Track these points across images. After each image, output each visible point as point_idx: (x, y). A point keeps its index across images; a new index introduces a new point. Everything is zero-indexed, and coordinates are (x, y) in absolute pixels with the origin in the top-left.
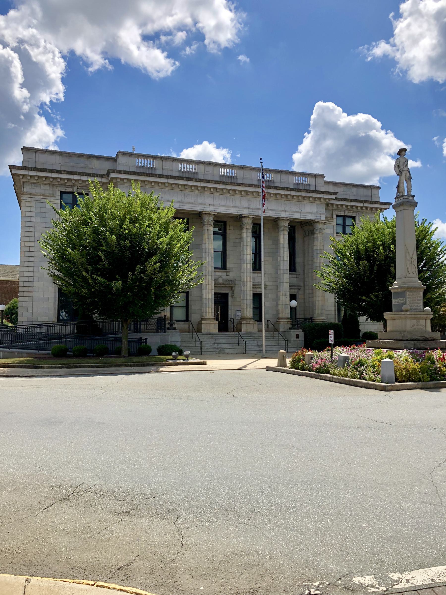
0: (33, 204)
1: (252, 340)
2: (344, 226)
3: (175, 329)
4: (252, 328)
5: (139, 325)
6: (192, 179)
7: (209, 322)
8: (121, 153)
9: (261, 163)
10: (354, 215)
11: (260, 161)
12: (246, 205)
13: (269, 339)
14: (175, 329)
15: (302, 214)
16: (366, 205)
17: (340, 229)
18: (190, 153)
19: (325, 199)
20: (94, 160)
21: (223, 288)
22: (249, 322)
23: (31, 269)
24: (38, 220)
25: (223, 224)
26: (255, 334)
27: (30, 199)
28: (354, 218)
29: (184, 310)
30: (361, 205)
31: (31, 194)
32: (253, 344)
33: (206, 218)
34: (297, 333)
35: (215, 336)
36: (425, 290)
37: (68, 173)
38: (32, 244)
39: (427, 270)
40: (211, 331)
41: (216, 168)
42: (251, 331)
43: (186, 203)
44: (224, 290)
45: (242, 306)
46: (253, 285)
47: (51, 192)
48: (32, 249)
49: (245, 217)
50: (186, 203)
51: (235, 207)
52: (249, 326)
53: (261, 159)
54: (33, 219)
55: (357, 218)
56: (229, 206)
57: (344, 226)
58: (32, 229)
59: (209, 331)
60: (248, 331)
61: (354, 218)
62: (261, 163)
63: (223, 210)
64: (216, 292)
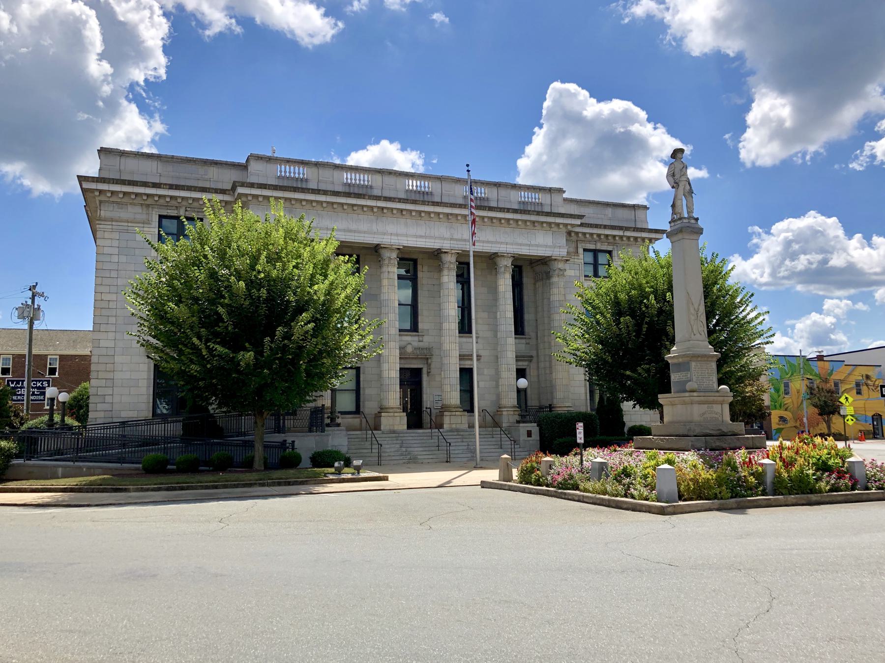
0: (116, 235)
2: (596, 265)
3: (338, 425)
7: (392, 414)
9: (468, 171)
10: (610, 248)
12: (447, 235)
14: (338, 425)
16: (628, 234)
17: (590, 271)
19: (566, 225)
23: (111, 335)
24: (123, 259)
25: (411, 263)
27: (110, 227)
28: (610, 252)
30: (621, 233)
31: (112, 220)
33: (386, 254)
34: (529, 429)
37: (171, 187)
38: (114, 297)
42: (458, 426)
46: (460, 355)
47: (144, 217)
48: (112, 305)
52: (454, 420)
53: (468, 165)
54: (115, 259)
55: (614, 253)
56: (421, 237)
57: (596, 265)
58: (114, 274)
59: (392, 428)
60: (454, 426)
61: (610, 252)
62: (468, 171)
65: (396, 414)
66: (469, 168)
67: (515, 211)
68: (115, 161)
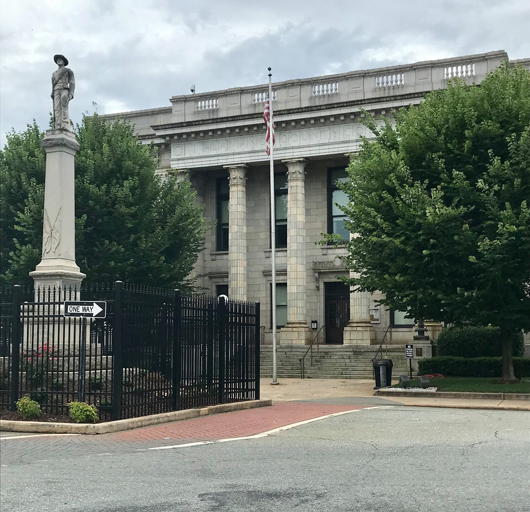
4: (361, 338)
8: (175, 100)
15: (294, 150)
22: (355, 329)
35: (294, 350)
36: (84, 279)
43: (258, 152)
52: (354, 336)
53: (270, 69)
59: (290, 342)
65: (294, 329)
66: (271, 72)
67: (371, 101)
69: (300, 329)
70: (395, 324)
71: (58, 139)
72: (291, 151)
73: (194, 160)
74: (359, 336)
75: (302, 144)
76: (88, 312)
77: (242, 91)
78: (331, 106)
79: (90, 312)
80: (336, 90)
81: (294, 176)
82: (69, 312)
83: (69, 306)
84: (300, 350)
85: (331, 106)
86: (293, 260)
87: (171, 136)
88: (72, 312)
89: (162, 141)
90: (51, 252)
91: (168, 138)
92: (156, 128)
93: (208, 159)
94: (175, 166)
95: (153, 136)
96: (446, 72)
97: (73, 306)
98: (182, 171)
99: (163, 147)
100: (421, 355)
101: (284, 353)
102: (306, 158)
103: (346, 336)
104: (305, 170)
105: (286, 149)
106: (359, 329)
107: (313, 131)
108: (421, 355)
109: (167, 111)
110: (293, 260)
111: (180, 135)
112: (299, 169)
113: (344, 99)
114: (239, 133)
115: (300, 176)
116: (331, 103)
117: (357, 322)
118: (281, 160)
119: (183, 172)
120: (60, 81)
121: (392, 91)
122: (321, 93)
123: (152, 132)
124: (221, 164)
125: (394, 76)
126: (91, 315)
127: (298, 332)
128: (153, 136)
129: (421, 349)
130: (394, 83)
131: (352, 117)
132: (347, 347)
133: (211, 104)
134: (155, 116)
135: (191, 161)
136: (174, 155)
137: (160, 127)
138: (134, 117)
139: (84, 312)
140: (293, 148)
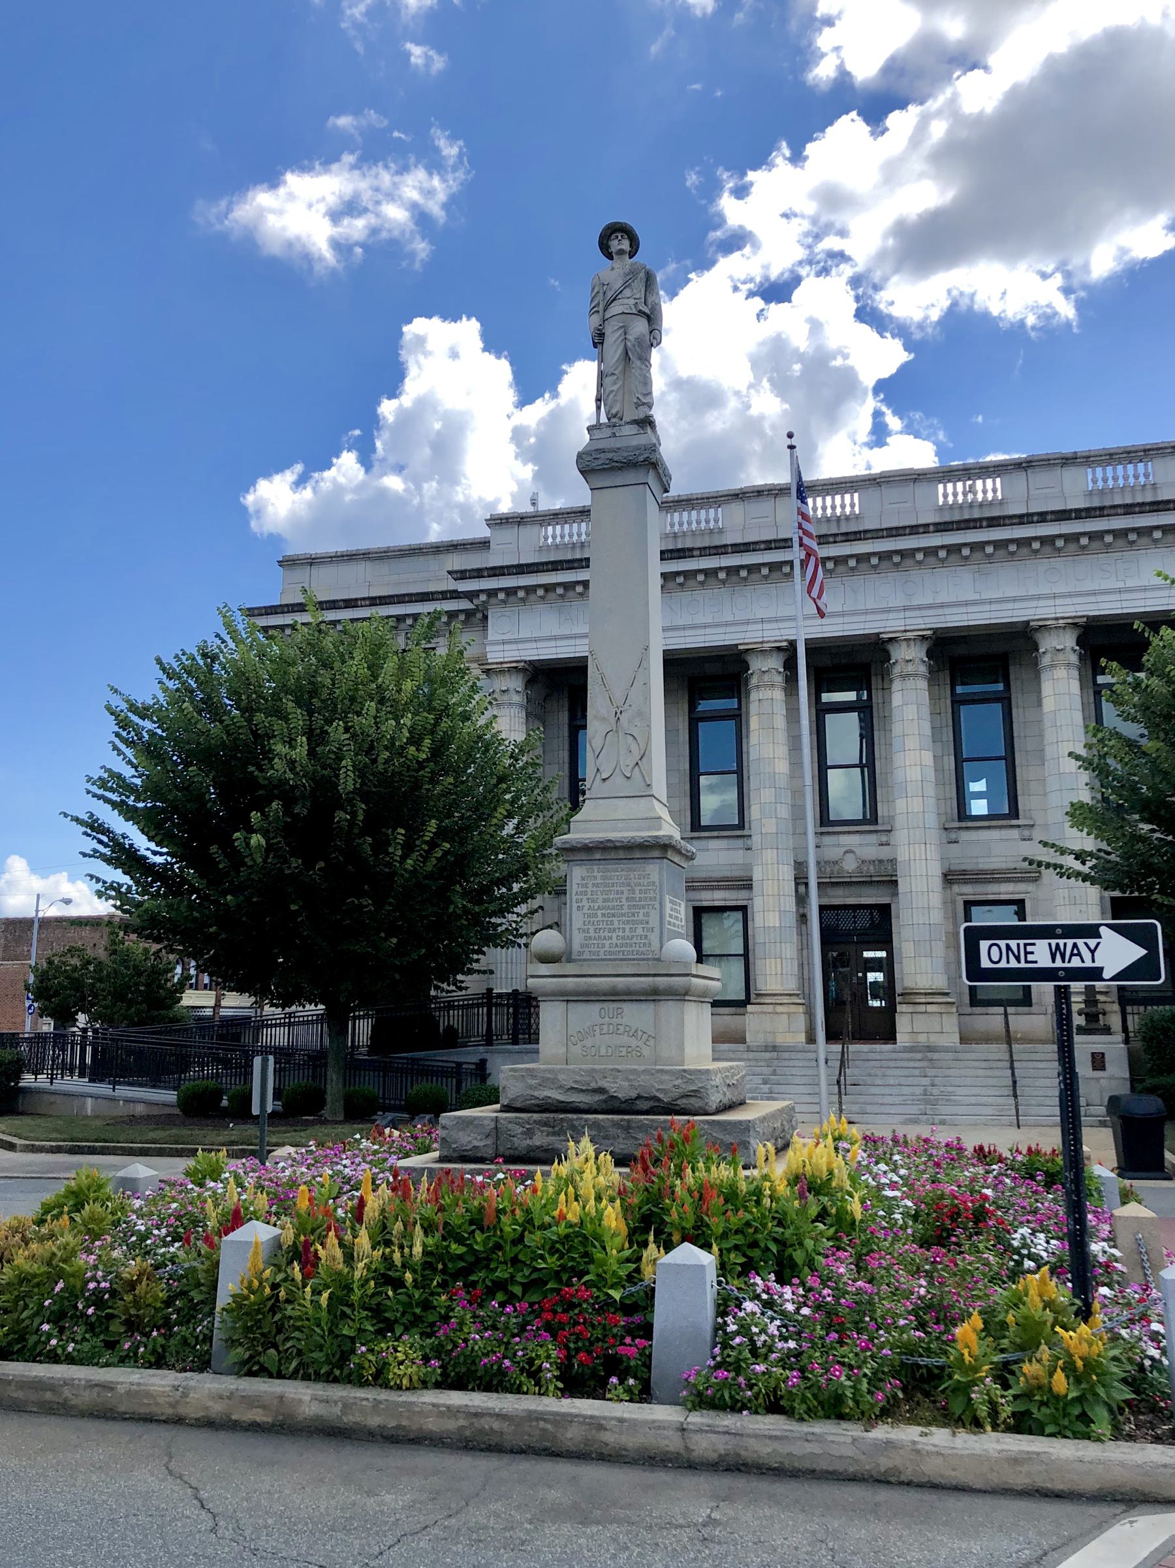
1: (917, 1072)
5: (88, 1060)
6: (691, 550)
7: (770, 1008)
9: (791, 447)
11: (789, 442)
13: (989, 1073)
15: (766, 626)
18: (988, 459)
20: (450, 555)
21: (866, 890)
22: (922, 1008)
25: (847, 669)
26: (946, 1050)
29: (737, 967)
32: (906, 1090)
34: (1098, 1048)
35: (786, 1055)
39: (433, 845)
40: (780, 1040)
41: (921, 489)
43: (684, 628)
44: (839, 897)
45: (923, 952)
49: (891, 639)
50: (684, 628)
51: (854, 613)
52: (921, 1023)
53: (790, 436)
59: (770, 1039)
60: (922, 1039)
62: (791, 447)
63: (979, 616)
64: (826, 901)
65: (780, 1009)
66: (794, 442)
68: (302, 575)
69: (793, 1008)
70: (979, 997)
71: (638, 448)
72: (759, 626)
73: (539, 645)
74: (934, 1023)
75: (942, 598)
76: (1076, 963)
77: (1069, 461)
78: (706, 551)
79: (1088, 964)
80: (716, 521)
81: (766, 677)
82: (985, 963)
83: (984, 945)
84: (799, 1055)
85: (706, 551)
86: (770, 855)
87: (492, 593)
88: (1003, 964)
89: (464, 604)
90: (618, 779)
91: (483, 597)
92: (462, 575)
93: (572, 642)
94: (495, 655)
95: (454, 595)
96: (669, 520)
97: (1002, 943)
98: (514, 665)
99: (462, 617)
100: (1103, 1068)
101: (778, 1072)
102: (935, 630)
103: (903, 1024)
104: (929, 654)
105: (748, 622)
106: (930, 1008)
107: (1043, 565)
108: (1103, 1068)
109: (484, 544)
110: (770, 855)
111: (511, 592)
112: (1068, 640)
113: (729, 539)
114: (504, 602)
115: (517, 699)
116: (718, 544)
117: (926, 994)
118: (736, 645)
119: (514, 669)
120: (627, 293)
121: (843, 524)
122: (703, 525)
123: (452, 585)
124: (1026, 619)
125: (703, 512)
126: (1095, 973)
127: (789, 1013)
128: (454, 595)
129: (1103, 1054)
130: (694, 526)
131: (897, 559)
132: (912, 1049)
133: (575, 530)
134: (441, 556)
135: (534, 645)
136: (493, 633)
137: (831, 539)
138: (395, 557)
139: (1059, 963)
140: (762, 621)
